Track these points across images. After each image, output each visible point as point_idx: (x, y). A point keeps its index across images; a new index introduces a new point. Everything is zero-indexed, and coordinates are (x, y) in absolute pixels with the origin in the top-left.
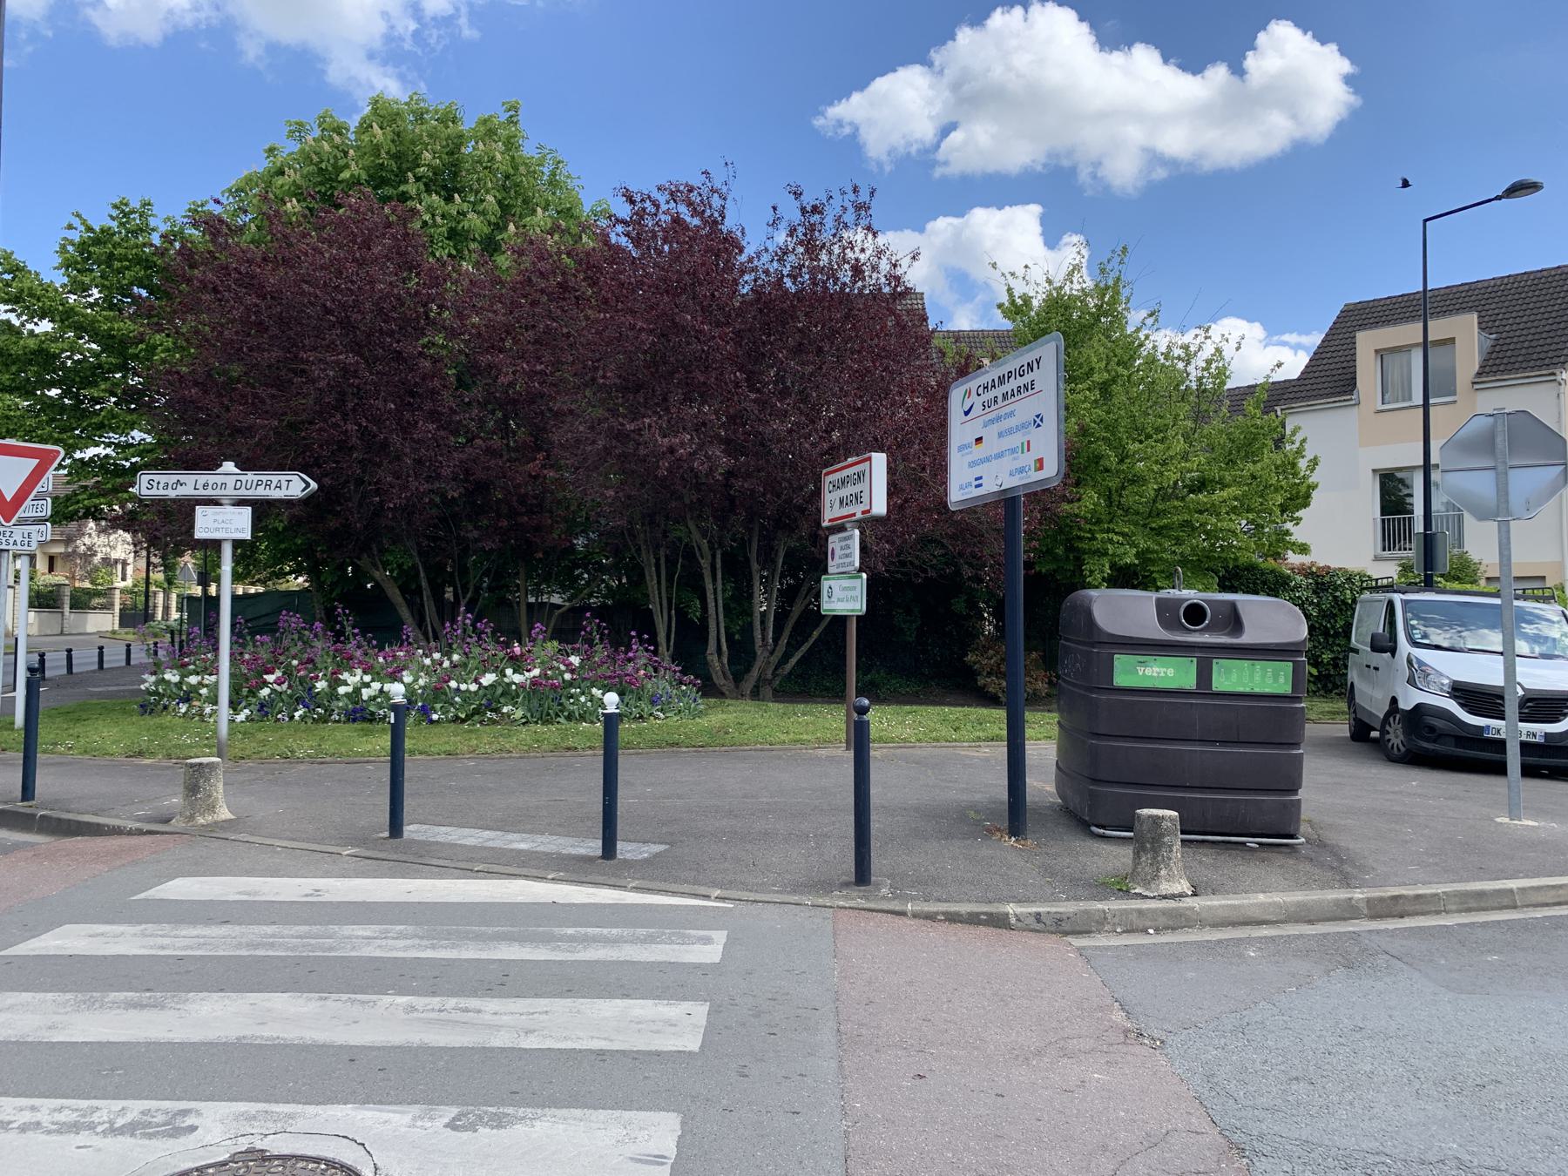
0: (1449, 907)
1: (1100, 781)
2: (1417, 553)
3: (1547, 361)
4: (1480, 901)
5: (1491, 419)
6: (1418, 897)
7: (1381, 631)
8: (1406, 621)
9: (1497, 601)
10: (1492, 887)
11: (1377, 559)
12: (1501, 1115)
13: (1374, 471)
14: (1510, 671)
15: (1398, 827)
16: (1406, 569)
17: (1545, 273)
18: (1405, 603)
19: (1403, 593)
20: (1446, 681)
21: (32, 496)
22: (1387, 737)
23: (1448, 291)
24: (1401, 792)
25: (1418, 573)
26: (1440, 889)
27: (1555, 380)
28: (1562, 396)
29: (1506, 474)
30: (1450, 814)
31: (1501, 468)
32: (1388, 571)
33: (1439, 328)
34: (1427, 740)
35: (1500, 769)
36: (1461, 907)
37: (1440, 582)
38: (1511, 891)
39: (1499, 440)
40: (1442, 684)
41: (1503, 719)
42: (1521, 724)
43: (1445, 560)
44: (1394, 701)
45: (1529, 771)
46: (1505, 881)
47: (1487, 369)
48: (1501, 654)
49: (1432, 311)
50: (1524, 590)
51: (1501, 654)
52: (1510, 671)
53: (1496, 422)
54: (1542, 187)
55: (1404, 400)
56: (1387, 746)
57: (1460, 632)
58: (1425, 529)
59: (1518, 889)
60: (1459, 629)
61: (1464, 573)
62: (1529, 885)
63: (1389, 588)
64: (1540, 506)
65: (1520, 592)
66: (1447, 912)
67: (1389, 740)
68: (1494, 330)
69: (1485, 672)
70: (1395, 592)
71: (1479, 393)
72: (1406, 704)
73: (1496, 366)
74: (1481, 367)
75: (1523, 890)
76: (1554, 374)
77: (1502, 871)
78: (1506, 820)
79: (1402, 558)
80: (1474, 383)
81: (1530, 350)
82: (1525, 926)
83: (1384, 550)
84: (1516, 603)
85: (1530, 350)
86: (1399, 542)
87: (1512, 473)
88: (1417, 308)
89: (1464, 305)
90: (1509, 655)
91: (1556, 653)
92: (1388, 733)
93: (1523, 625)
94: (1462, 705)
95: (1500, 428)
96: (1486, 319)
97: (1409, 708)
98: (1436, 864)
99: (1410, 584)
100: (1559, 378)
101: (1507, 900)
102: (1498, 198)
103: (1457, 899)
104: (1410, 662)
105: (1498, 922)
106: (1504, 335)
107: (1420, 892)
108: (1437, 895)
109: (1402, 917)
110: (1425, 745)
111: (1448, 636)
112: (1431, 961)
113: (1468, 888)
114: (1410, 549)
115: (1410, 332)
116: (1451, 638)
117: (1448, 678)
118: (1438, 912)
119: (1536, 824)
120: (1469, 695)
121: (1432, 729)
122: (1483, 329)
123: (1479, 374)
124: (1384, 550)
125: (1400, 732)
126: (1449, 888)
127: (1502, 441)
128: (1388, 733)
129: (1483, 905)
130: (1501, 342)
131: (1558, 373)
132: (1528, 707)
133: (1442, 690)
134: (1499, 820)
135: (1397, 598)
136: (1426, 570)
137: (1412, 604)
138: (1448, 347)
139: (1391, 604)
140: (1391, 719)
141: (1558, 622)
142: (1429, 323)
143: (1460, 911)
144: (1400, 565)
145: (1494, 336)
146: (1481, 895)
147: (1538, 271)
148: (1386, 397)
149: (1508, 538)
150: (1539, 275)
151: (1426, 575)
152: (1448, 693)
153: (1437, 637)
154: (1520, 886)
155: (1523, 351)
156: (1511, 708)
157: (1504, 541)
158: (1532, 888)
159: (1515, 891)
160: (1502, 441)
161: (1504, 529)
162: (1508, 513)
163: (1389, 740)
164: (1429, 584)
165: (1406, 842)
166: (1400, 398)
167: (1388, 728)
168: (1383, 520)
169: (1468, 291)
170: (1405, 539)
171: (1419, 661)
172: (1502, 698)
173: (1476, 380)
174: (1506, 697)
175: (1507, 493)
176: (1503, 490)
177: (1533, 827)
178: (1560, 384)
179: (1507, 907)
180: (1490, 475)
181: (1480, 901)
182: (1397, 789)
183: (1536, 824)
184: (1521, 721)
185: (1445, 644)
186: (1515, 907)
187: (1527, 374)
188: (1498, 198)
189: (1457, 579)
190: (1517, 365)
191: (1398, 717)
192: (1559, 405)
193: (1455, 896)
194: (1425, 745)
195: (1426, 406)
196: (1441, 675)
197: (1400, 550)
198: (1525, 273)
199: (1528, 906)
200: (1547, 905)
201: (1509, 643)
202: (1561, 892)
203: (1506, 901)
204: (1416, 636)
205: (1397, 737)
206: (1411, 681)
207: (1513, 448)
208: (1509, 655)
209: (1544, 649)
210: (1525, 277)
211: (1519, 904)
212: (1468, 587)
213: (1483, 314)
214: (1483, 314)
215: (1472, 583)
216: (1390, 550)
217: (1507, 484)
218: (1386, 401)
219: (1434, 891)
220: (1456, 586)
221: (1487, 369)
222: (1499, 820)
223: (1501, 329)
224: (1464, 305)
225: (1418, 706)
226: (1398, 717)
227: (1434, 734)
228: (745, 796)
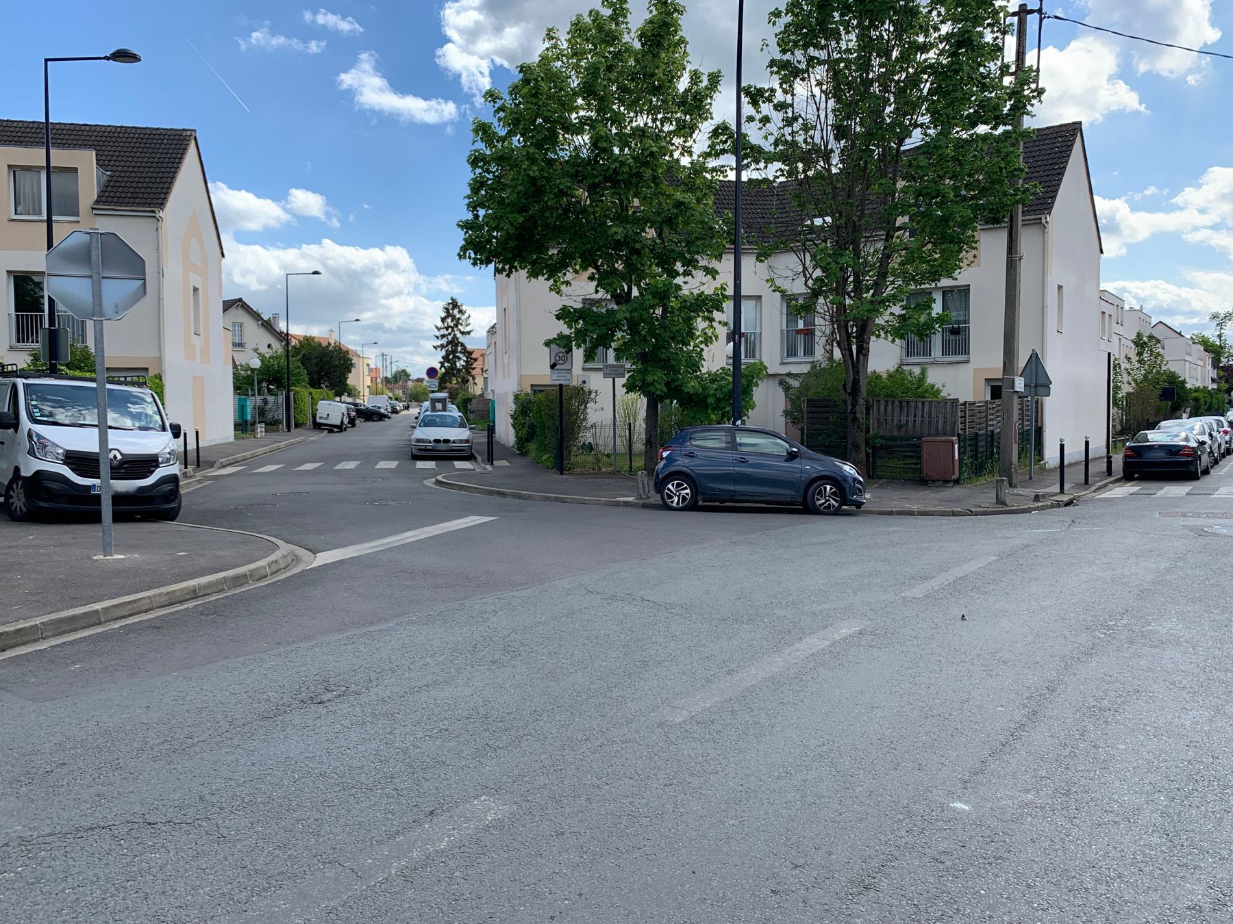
0: (45, 634)
1: (891, 513)
2: (43, 346)
3: (149, 201)
4: (73, 624)
5: (87, 237)
6: (18, 631)
7: (6, 410)
8: (27, 404)
9: (94, 385)
10: (81, 612)
11: (12, 349)
12: (62, 790)
13: (9, 272)
14: (103, 440)
15: (9, 576)
16: (36, 358)
17: (148, 131)
18: (26, 386)
19: (25, 378)
20: (61, 451)
21: (1217, 418)
22: (11, 501)
23: (72, 127)
24: (17, 546)
25: (43, 364)
26: (37, 621)
27: (154, 217)
28: (159, 229)
29: (100, 282)
30: (58, 558)
31: (95, 277)
32: (22, 360)
33: (61, 157)
34: (46, 501)
35: (96, 518)
36: (55, 632)
37: (63, 370)
38: (97, 612)
39: (94, 254)
40: (58, 454)
41: (99, 478)
42: (112, 481)
43: (66, 354)
44: (17, 469)
45: (118, 518)
46: (92, 605)
47: (104, 199)
48: (110, 427)
49: (54, 141)
50: (126, 377)
51: (110, 427)
52: (103, 440)
53: (91, 239)
54: (139, 60)
55: (34, 214)
56: (11, 509)
57: (80, 410)
58: (50, 325)
59: (102, 609)
60: (80, 408)
61: (84, 363)
62: (111, 604)
63: (15, 374)
64: (127, 310)
65: (123, 379)
66: (44, 639)
67: (13, 503)
68: (109, 168)
69: (85, 441)
70: (18, 377)
71: (98, 218)
72: (26, 472)
73: (111, 198)
74: (98, 196)
75: (106, 609)
76: (154, 212)
77: (91, 597)
78: (101, 557)
79: (34, 350)
80: (93, 209)
81: (137, 190)
82: (105, 636)
83: (19, 341)
84: (109, 386)
85: (137, 190)
86: (32, 335)
87: (104, 282)
88: (40, 136)
89: (85, 143)
90: (103, 428)
91: (151, 426)
92: (12, 497)
93: (129, 405)
94: (73, 470)
95: (94, 244)
96: (103, 158)
97: (29, 474)
98: (38, 601)
99: (38, 371)
100: (157, 216)
101: (93, 619)
102: (105, 58)
103: (53, 627)
104: (30, 435)
105: (85, 638)
106: (117, 174)
107: (20, 626)
108: (36, 625)
109: (4, 651)
110: (42, 504)
111: (69, 414)
112: (23, 681)
113: (62, 616)
114: (37, 342)
115: (34, 156)
116: (72, 415)
117: (61, 448)
118: (36, 640)
119: (123, 557)
120: (75, 460)
121: (49, 490)
122: (101, 166)
123: (97, 202)
124: (19, 341)
125: (22, 496)
126: (45, 619)
127: (96, 255)
128: (12, 497)
129: (74, 626)
130: (115, 179)
131: (157, 211)
132: (125, 468)
133: (57, 458)
134: (95, 558)
135: (20, 382)
136: (51, 359)
137: (33, 387)
138: (70, 176)
139: (14, 387)
140: (15, 486)
141: (151, 403)
142: (51, 151)
143: (54, 636)
144: (31, 355)
145: (109, 173)
146: (72, 619)
147: (143, 128)
148: (19, 208)
149: (102, 334)
150: (144, 131)
151: (51, 364)
152: (62, 460)
153: (61, 416)
154: (104, 606)
155: (131, 190)
156: (105, 469)
157: (99, 336)
158: (113, 606)
159: (100, 611)
160: (96, 255)
161: (98, 327)
162: (102, 314)
163: (13, 503)
164: (53, 372)
165: (14, 587)
166: (31, 212)
167: (11, 493)
168: (17, 316)
169: (88, 131)
170: (32, 335)
171: (39, 436)
172: (98, 460)
173: (95, 206)
174: (101, 460)
175: (100, 298)
176: (97, 295)
177: (121, 559)
178: (158, 220)
179: (93, 625)
180: (88, 281)
181: (73, 624)
182: (14, 544)
183: (123, 557)
184: (112, 479)
185: (67, 422)
186: (100, 624)
187: (134, 209)
188: (105, 58)
189: (80, 369)
190: (126, 200)
191: (20, 483)
192: (158, 235)
193: (51, 624)
194: (42, 504)
195: (49, 222)
196: (57, 446)
197: (33, 342)
198: (134, 127)
199: (109, 621)
200: (124, 617)
201: (103, 417)
202: (134, 605)
203: (92, 620)
204: (36, 414)
205: (19, 500)
206: (31, 452)
207: (106, 260)
208: (103, 428)
209: (143, 424)
210: (134, 131)
211: (103, 620)
212: (88, 375)
213: (101, 153)
214: (101, 153)
215: (91, 372)
216: (23, 342)
217: (100, 291)
218: (19, 212)
219: (33, 623)
220: (77, 373)
221: (104, 199)
222: (95, 558)
223: (114, 168)
224: (85, 143)
225: (38, 473)
226: (20, 483)
227: (51, 495)
228: (753, 543)
